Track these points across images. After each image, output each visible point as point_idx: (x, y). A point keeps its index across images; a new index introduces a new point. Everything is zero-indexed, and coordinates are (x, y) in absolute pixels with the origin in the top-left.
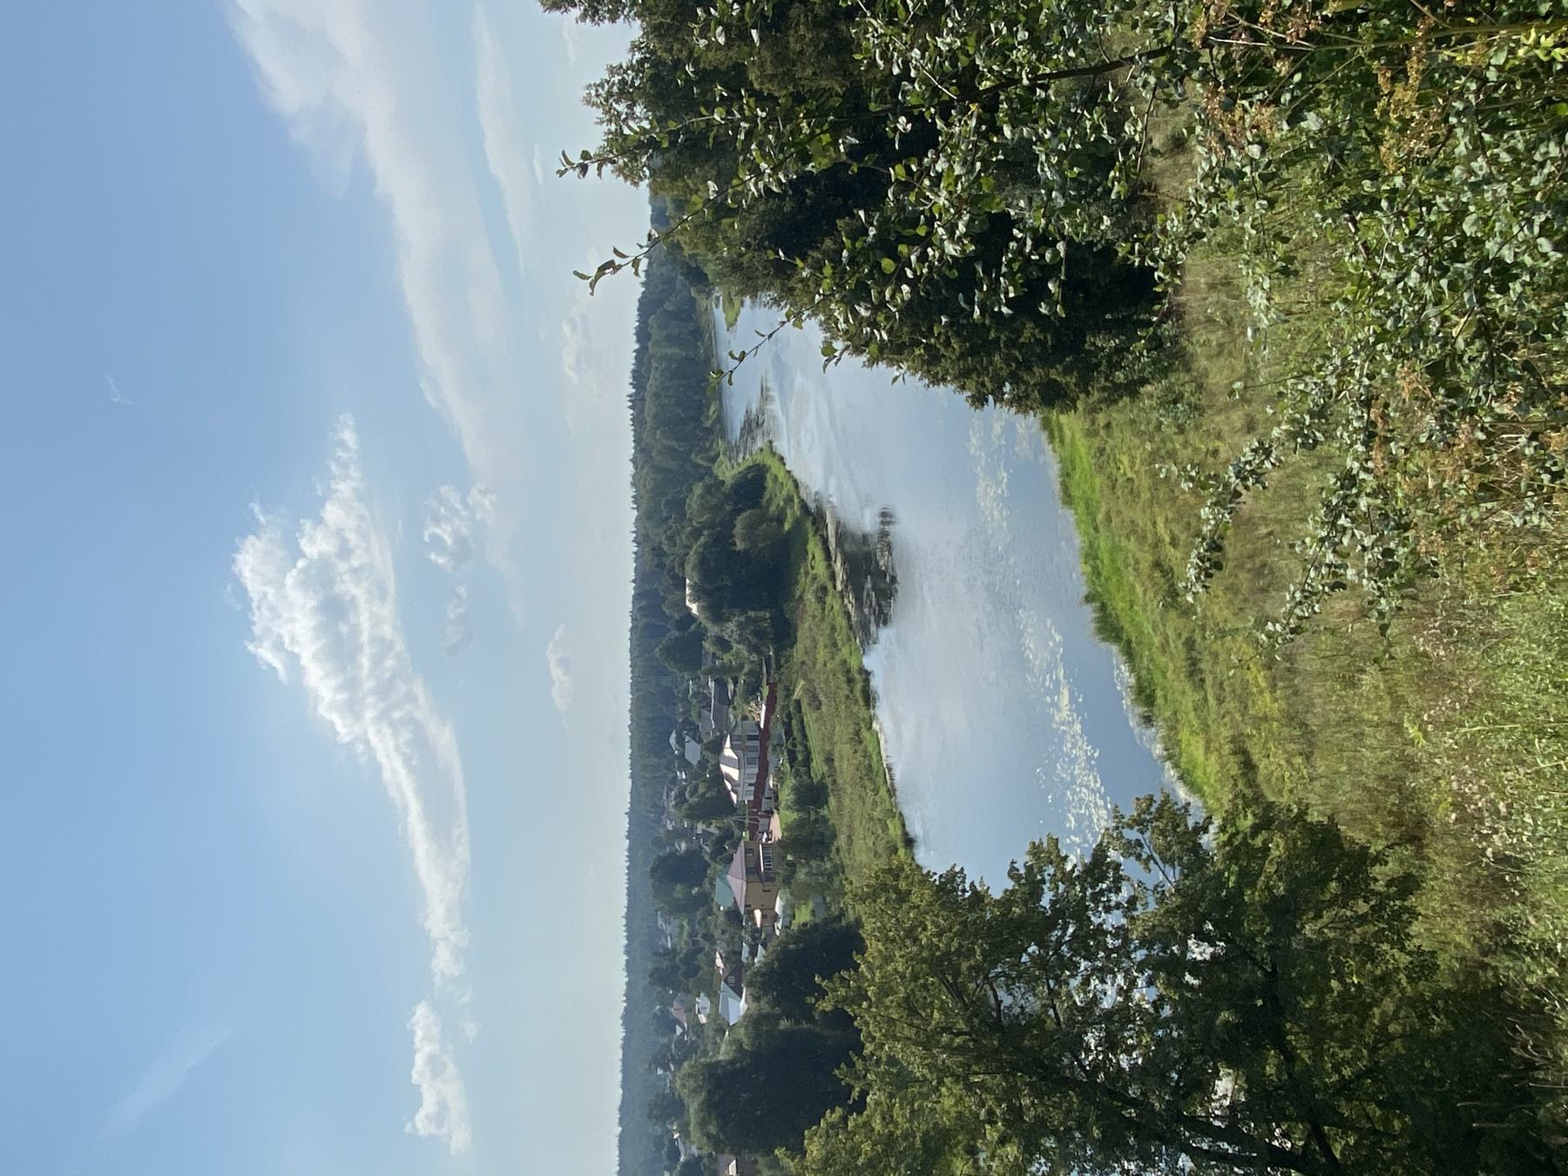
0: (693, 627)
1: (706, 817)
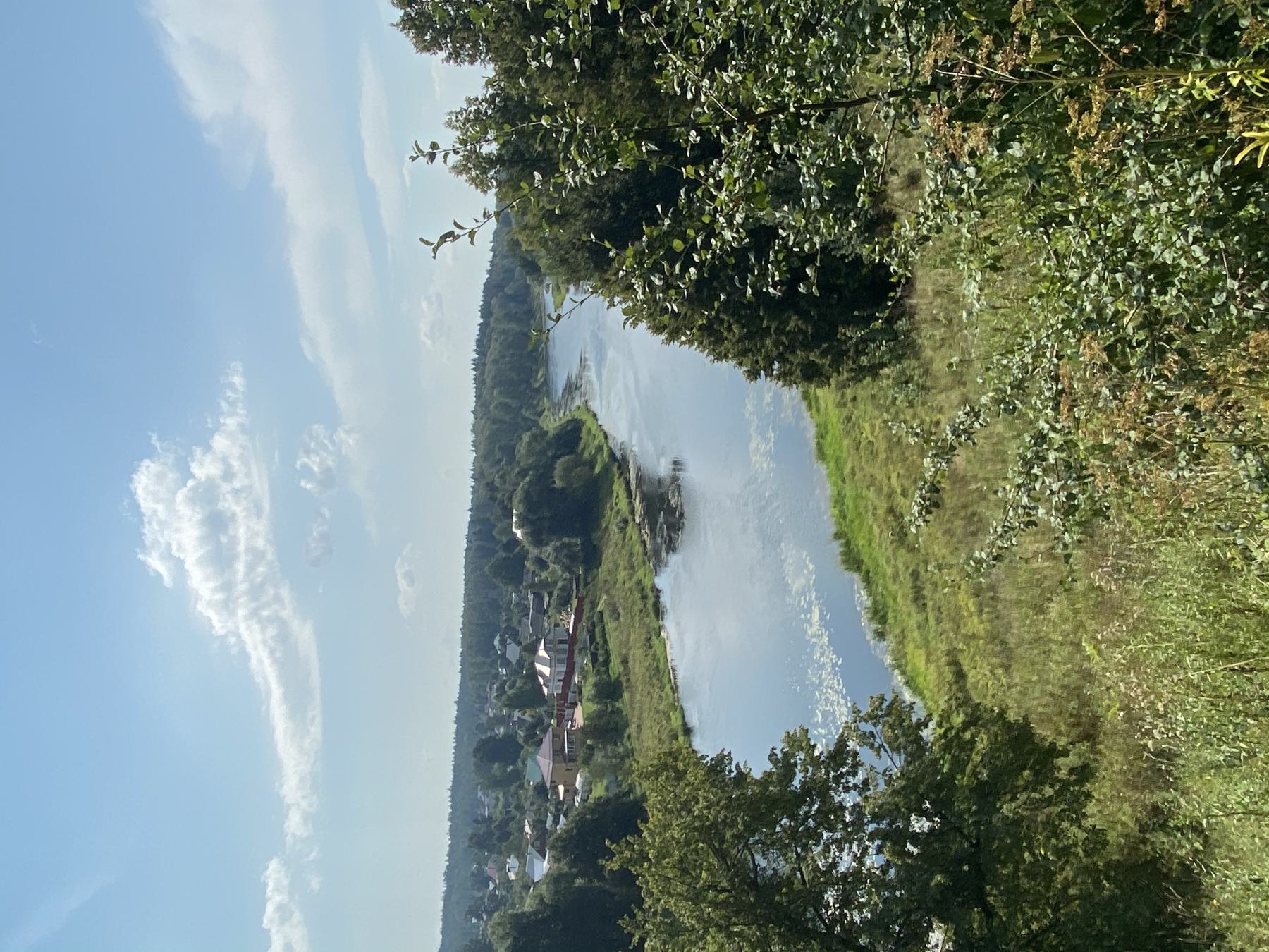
0: (517, 550)
1: (522, 707)
